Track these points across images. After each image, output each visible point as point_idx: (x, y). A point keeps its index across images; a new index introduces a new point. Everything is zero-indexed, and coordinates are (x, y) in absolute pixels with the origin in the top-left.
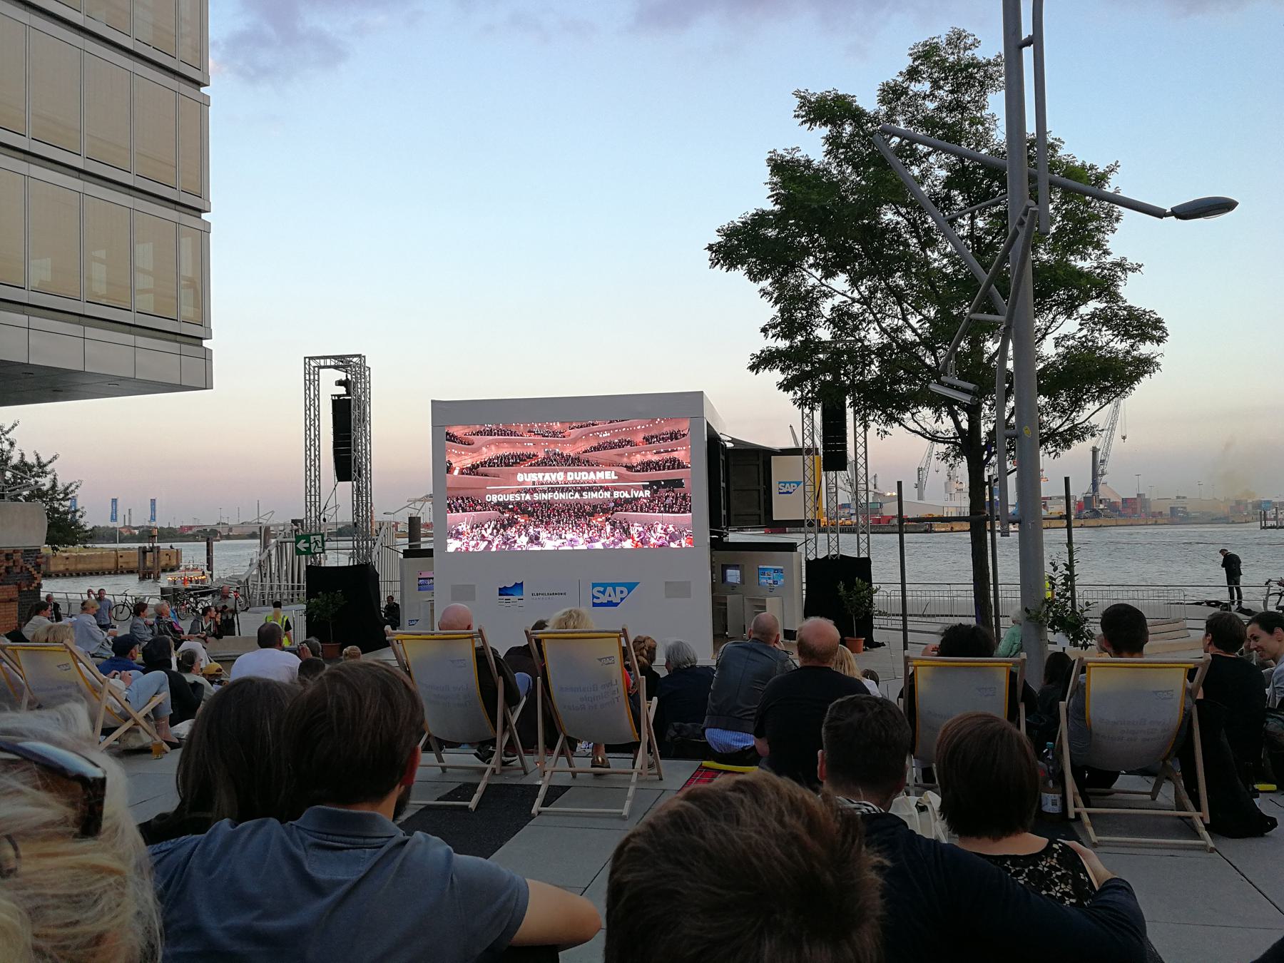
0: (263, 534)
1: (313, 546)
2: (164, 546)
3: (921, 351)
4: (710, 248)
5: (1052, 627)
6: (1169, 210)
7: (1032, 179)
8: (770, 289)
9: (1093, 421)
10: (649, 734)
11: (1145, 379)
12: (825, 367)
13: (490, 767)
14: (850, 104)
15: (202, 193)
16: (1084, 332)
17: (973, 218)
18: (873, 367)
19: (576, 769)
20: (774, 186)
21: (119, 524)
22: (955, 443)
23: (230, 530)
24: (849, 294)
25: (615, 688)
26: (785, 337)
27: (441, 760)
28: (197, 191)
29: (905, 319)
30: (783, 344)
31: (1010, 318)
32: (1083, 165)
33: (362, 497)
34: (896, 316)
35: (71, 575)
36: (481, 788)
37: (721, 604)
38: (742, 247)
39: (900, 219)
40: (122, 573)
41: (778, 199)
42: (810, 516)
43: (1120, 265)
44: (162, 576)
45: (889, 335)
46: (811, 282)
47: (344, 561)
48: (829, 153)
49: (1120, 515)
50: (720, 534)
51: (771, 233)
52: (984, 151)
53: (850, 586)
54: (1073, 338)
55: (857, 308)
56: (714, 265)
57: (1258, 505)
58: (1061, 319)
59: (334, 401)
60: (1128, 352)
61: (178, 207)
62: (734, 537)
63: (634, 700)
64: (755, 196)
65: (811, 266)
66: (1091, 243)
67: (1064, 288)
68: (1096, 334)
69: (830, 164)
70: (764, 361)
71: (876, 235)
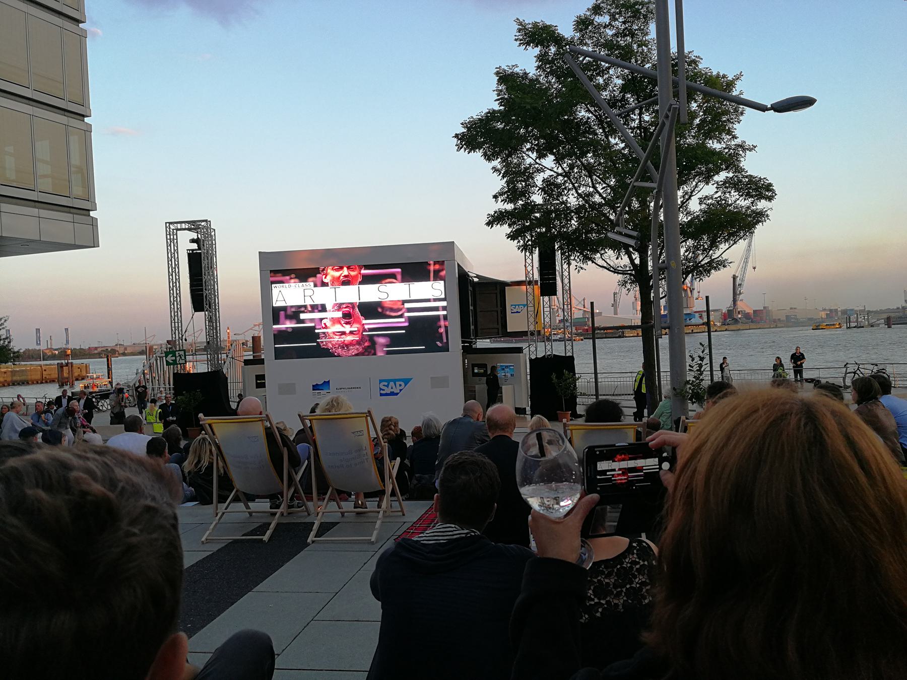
0: (147, 351)
1: (178, 359)
2: (76, 362)
3: (606, 210)
4: (456, 136)
5: (691, 399)
6: (769, 106)
7: (675, 85)
8: (499, 167)
9: (724, 256)
10: (393, 483)
11: (759, 227)
12: (539, 223)
13: (279, 511)
14: (554, 32)
15: (84, 102)
16: (719, 194)
17: (640, 114)
18: (573, 222)
19: (344, 510)
20: (499, 92)
21: (43, 347)
22: (631, 275)
23: (126, 349)
24: (555, 169)
25: (365, 452)
26: (511, 201)
27: (248, 507)
28: (80, 101)
29: (594, 187)
30: (510, 207)
31: (660, 185)
32: (718, 74)
33: (213, 323)
34: (588, 185)
35: (9, 385)
36: (272, 526)
37: (472, 391)
38: (477, 136)
39: (591, 115)
40: (46, 382)
41: (502, 102)
42: (532, 328)
43: (741, 146)
44: (76, 383)
45: (583, 199)
46: (529, 161)
47: (202, 368)
48: (538, 67)
49: (752, 322)
50: (470, 343)
51: (500, 126)
52: (647, 66)
53: (560, 376)
54: (712, 198)
55: (560, 180)
56: (459, 149)
57: (844, 312)
58: (701, 185)
59: (189, 254)
60: (748, 208)
61: (66, 113)
62: (483, 343)
63: (379, 461)
64: (485, 100)
65: (528, 150)
66: (724, 130)
67: (699, 163)
68: (727, 195)
69: (540, 76)
70: (497, 219)
71: (576, 128)
